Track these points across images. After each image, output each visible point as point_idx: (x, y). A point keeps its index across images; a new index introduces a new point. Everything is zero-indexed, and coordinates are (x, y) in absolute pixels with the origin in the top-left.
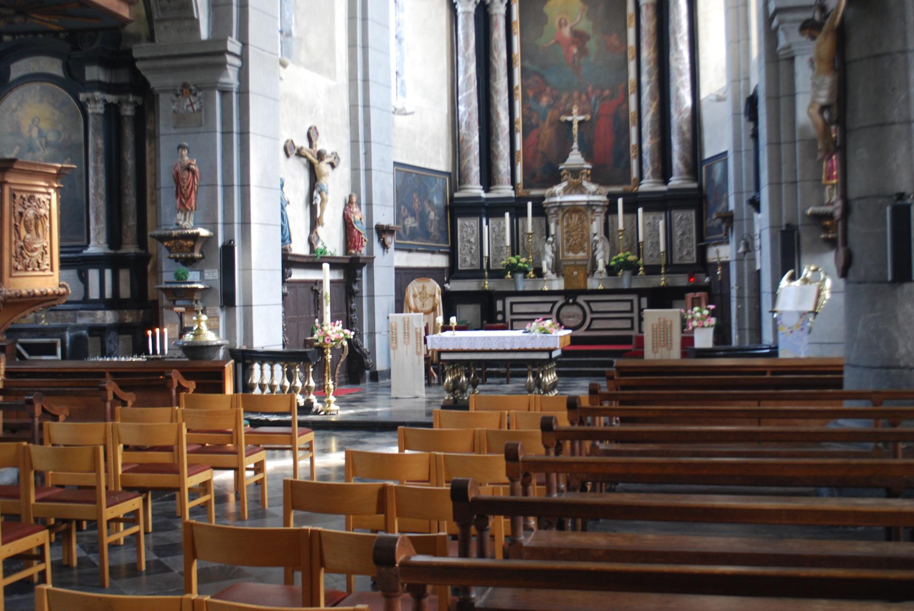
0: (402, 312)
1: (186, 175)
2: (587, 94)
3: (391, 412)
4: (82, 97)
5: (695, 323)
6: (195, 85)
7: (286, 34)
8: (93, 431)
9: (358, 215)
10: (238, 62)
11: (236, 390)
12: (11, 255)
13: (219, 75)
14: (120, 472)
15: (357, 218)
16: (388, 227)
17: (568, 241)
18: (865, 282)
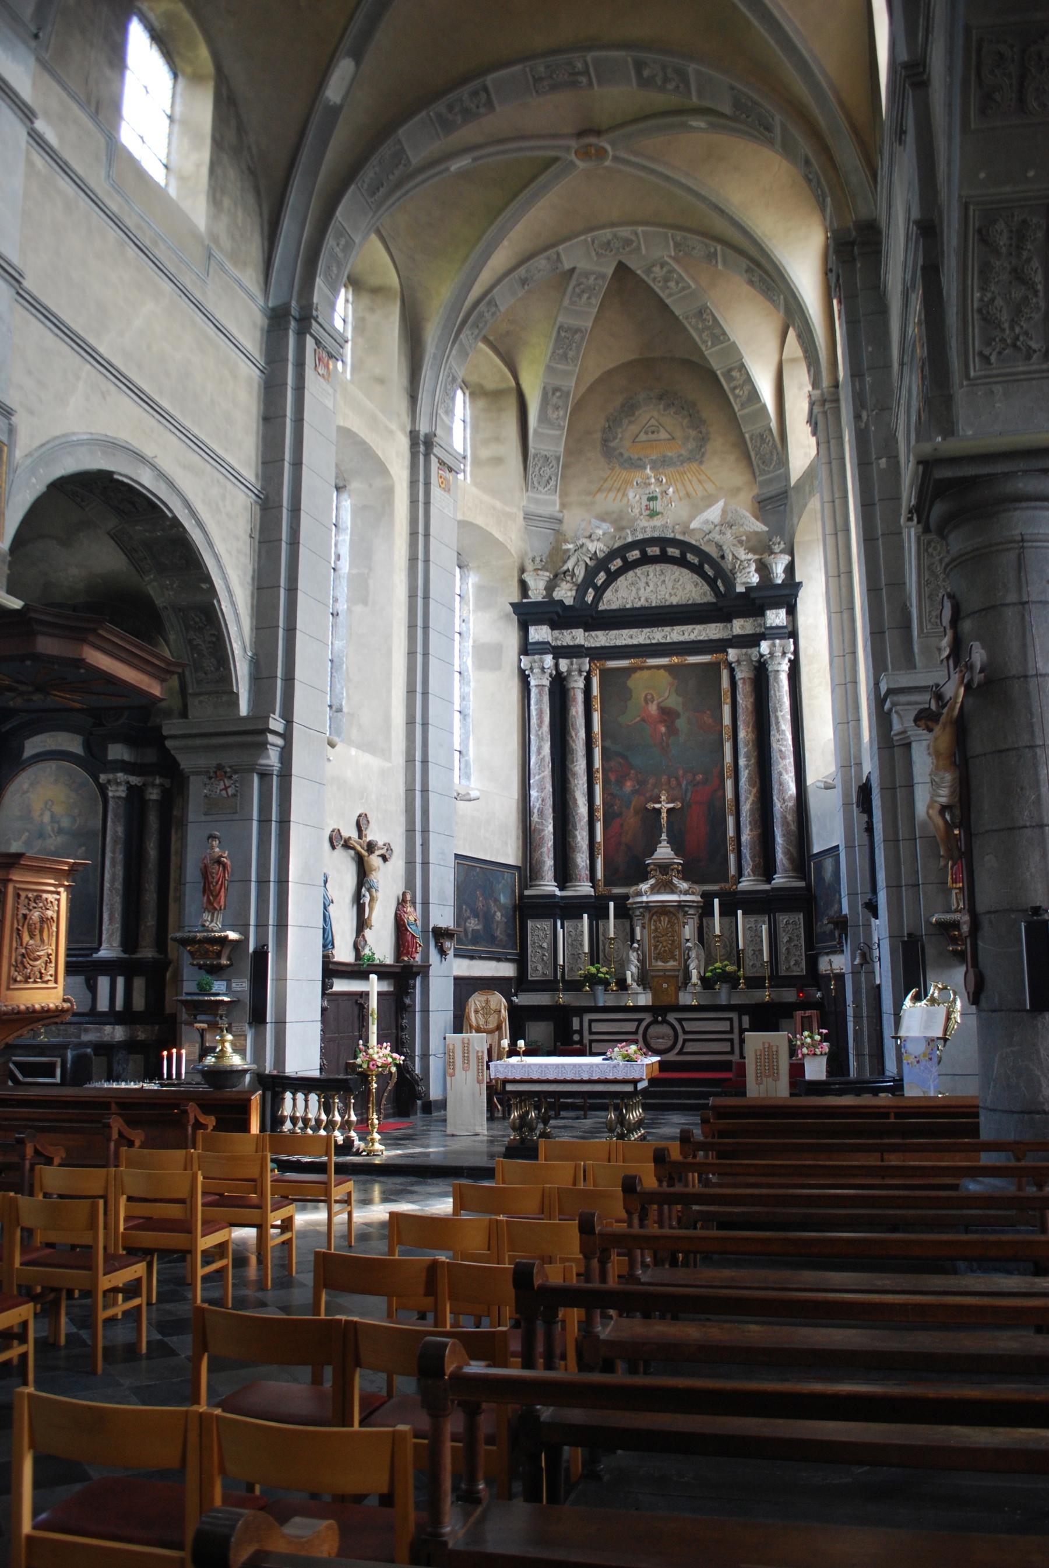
0: (461, 1032)
1: (215, 868)
2: (677, 779)
3: (445, 1153)
4: (103, 778)
5: (805, 1051)
6: (230, 767)
7: (336, 709)
8: (92, 1180)
9: (413, 915)
10: (280, 742)
11: (263, 1129)
12: (10, 965)
13: (259, 757)
14: (122, 1229)
15: (412, 919)
16: (447, 929)
17: (656, 947)
18: (1000, 1011)
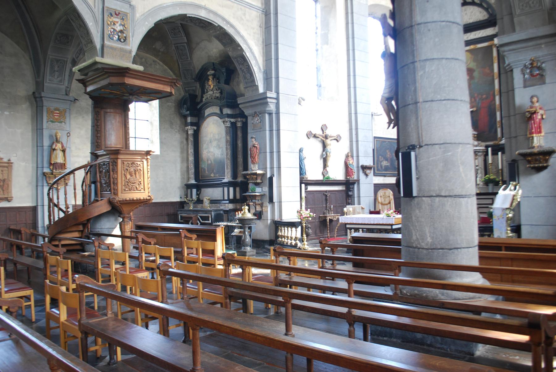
2: (474, 98)
10: (275, 101)
15: (351, 162)
